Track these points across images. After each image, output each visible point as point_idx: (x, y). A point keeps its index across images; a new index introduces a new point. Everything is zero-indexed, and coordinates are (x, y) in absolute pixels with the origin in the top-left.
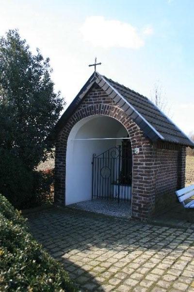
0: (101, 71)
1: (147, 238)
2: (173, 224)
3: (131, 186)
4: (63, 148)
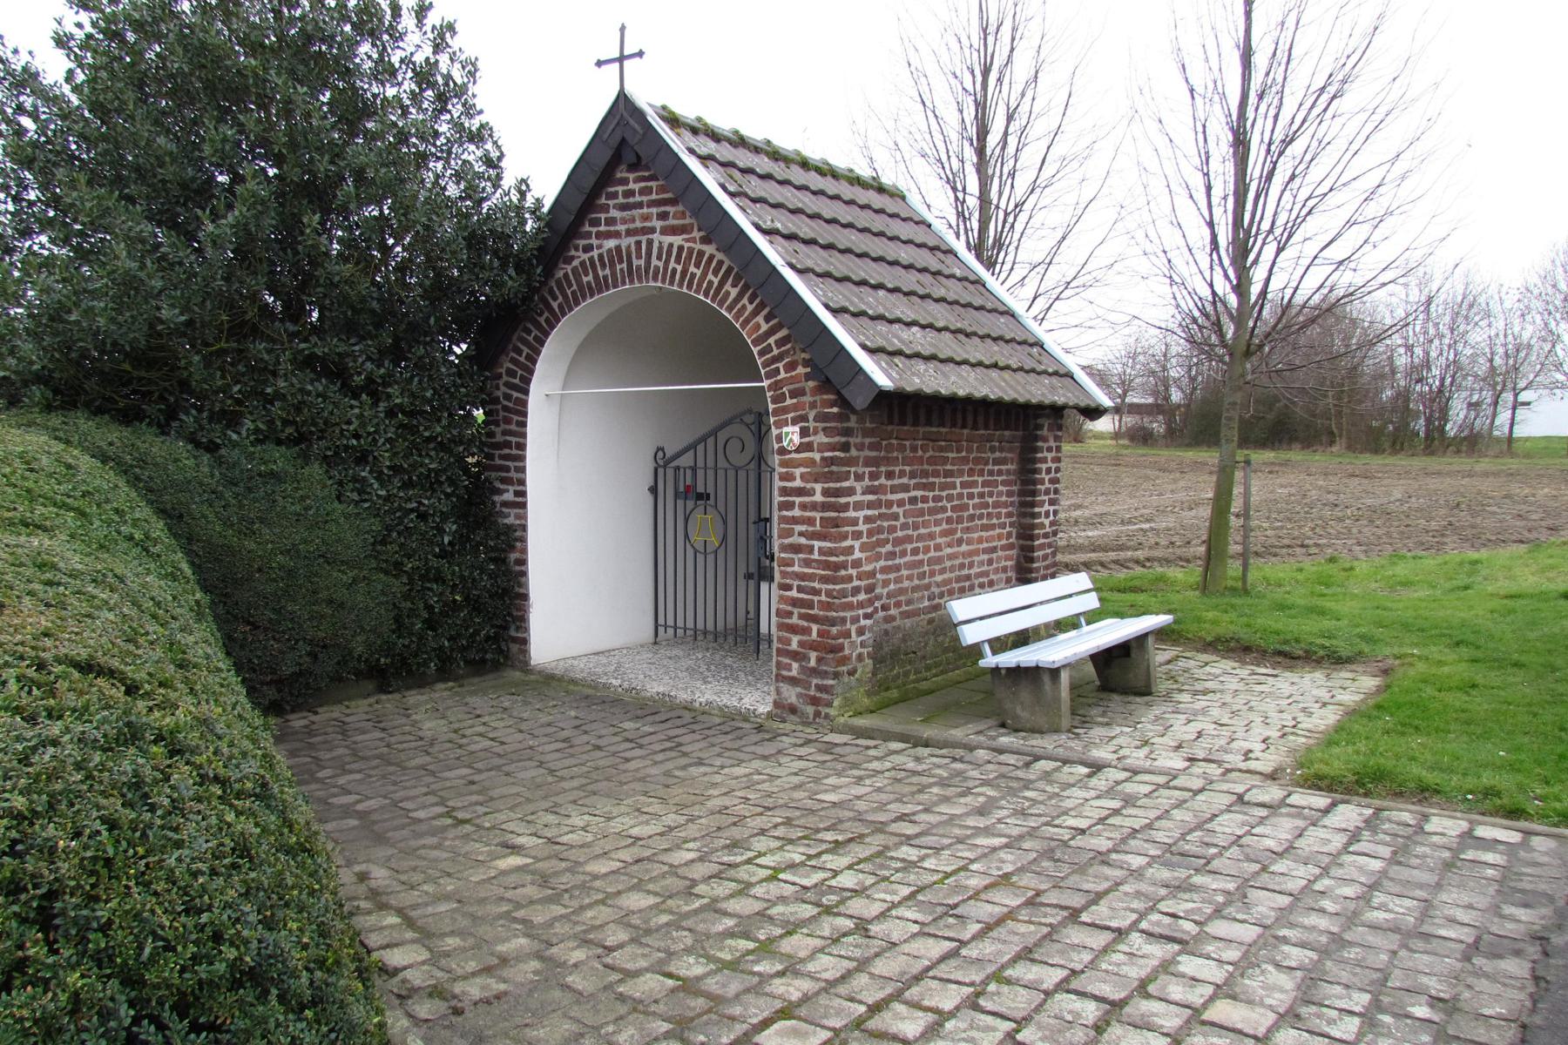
0: (646, 97)
2: (928, 732)
3: (771, 579)
4: (513, 427)
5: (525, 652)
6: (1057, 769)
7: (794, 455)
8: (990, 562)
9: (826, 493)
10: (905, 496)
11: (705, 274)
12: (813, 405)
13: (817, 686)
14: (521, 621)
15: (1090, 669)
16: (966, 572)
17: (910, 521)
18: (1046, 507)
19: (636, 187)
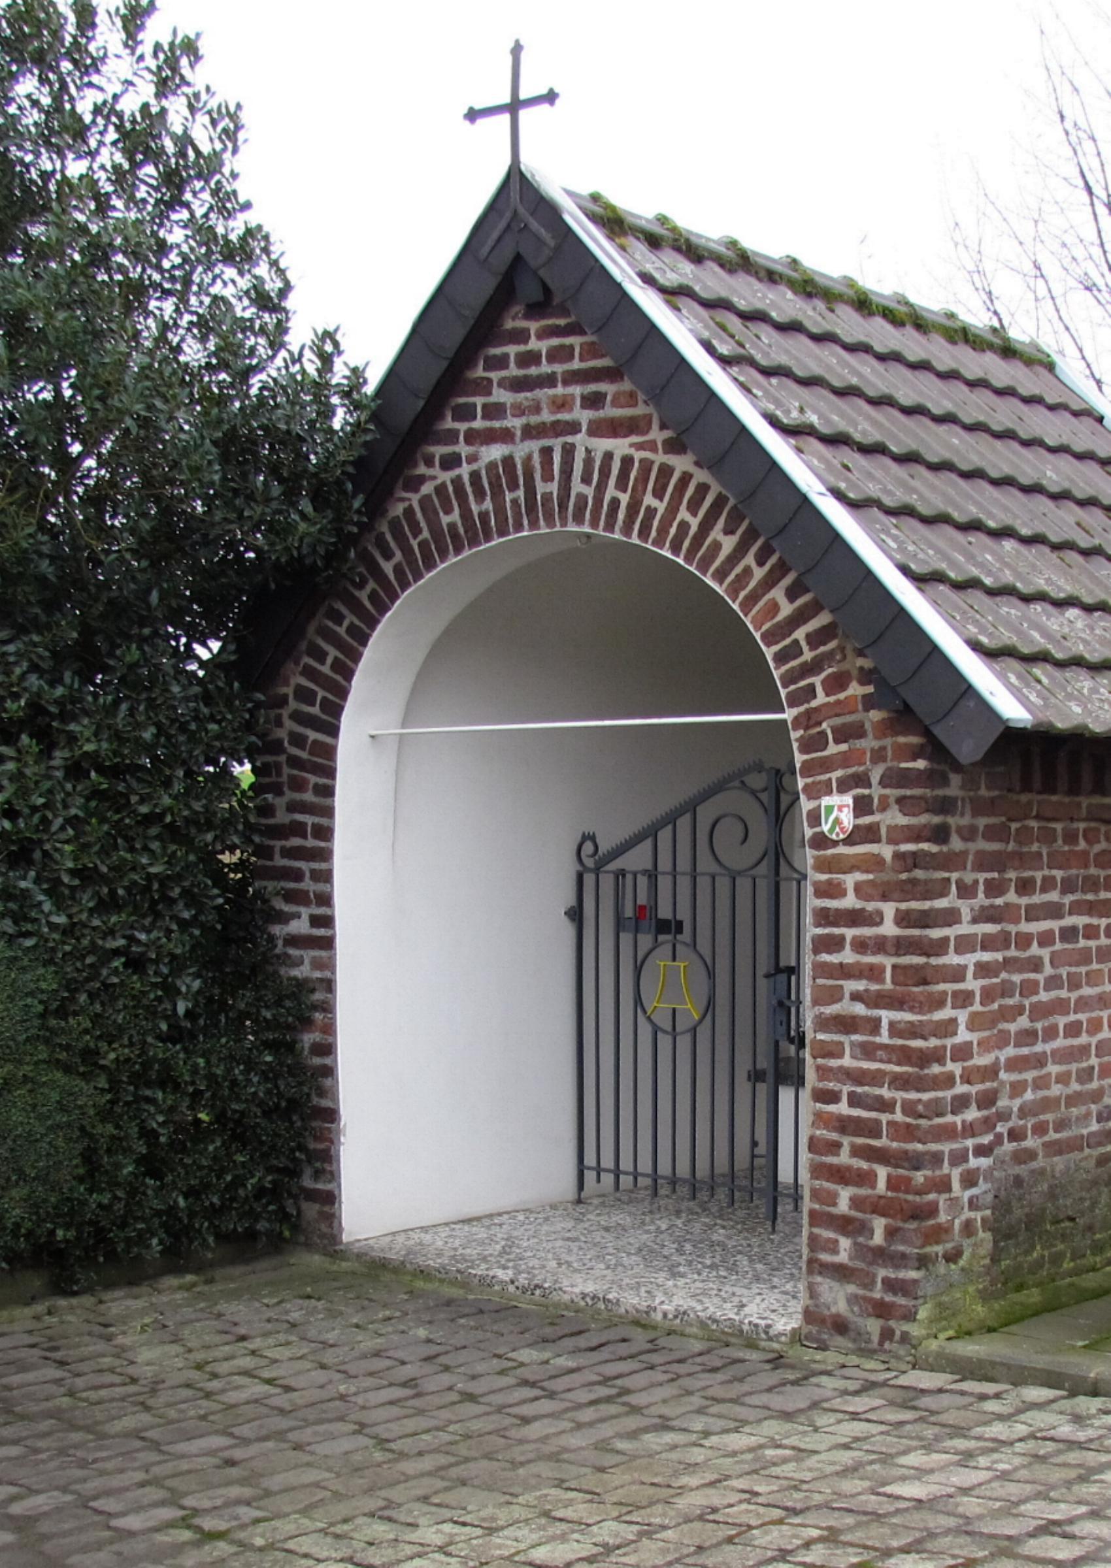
1: (232, 1401)
4: (309, 797)
7: (842, 850)
9: (903, 919)
10: (1054, 925)
11: (672, 510)
12: (878, 756)
13: (886, 1281)
17: (1064, 972)
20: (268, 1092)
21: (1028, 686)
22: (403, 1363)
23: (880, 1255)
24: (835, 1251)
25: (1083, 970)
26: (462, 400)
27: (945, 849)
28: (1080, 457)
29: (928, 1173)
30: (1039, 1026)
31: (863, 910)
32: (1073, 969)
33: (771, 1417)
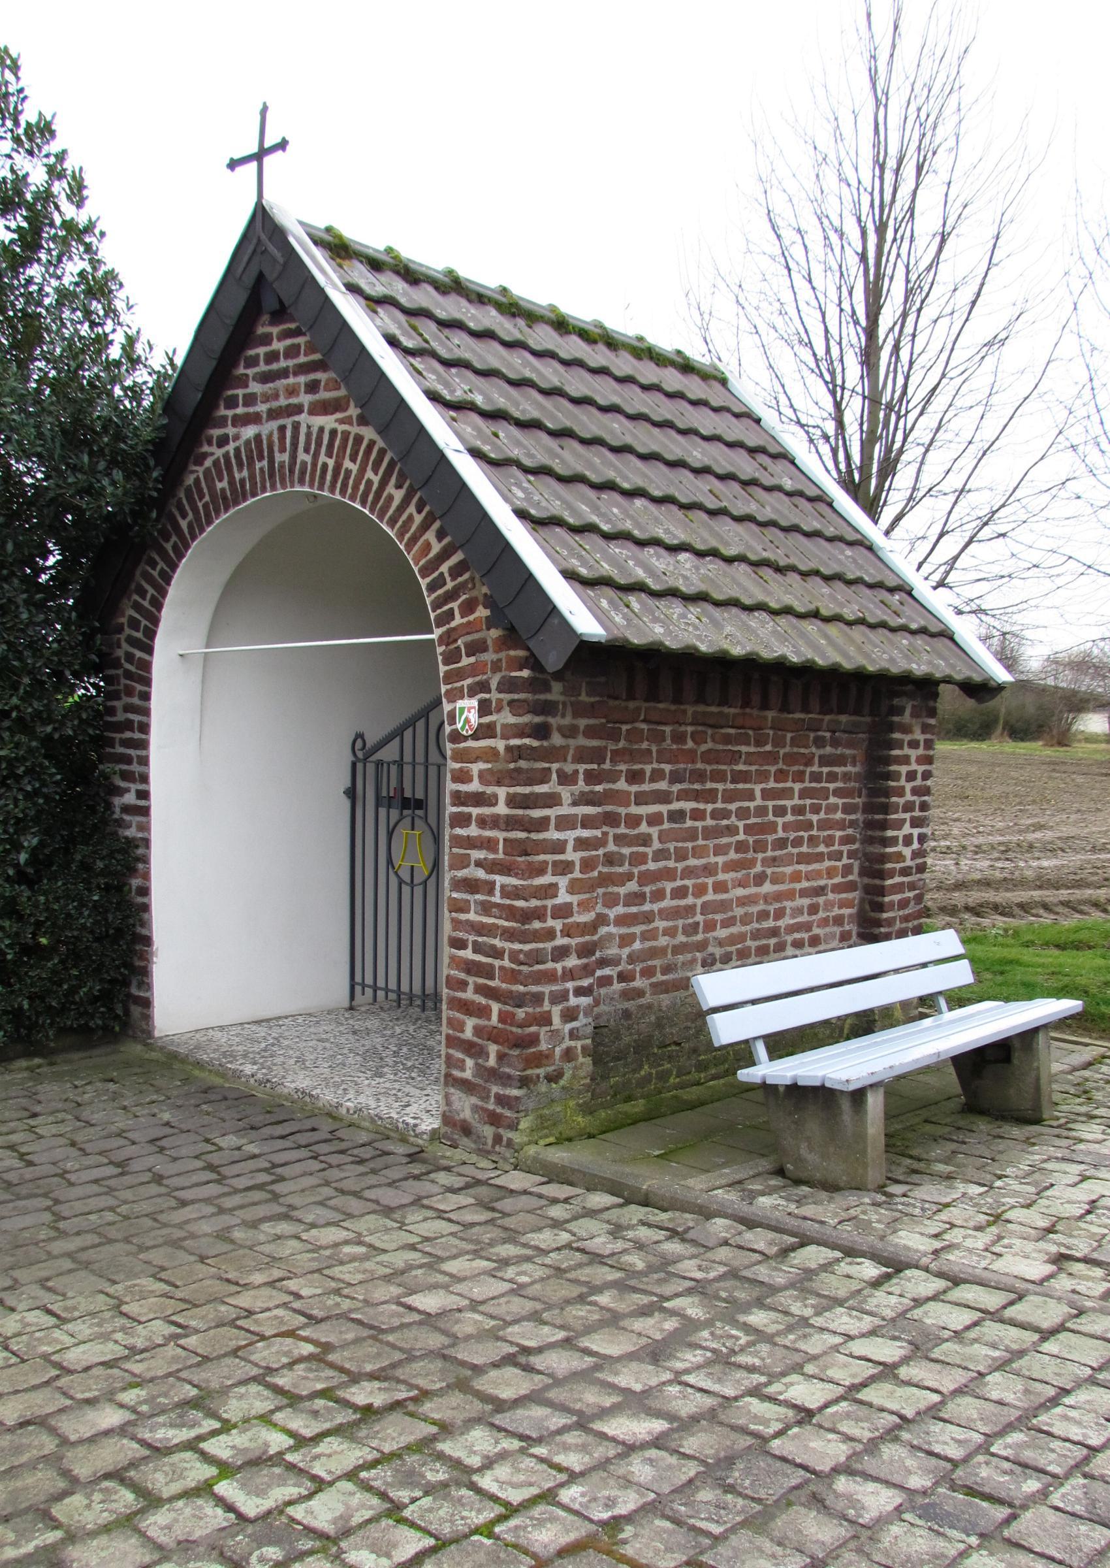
2: (651, 1180)
4: (136, 701)
5: (148, 1018)
6: (827, 1267)
7: (471, 744)
8: (813, 909)
9: (512, 801)
10: (663, 809)
11: (362, 471)
12: (496, 667)
13: (498, 1096)
14: (143, 974)
15: (951, 1080)
16: (770, 923)
17: (671, 846)
18: (907, 829)
19: (278, 346)
20: (96, 923)
21: (616, 609)
22: (134, 1143)
23: (493, 1075)
24: (463, 1070)
25: (690, 845)
26: (230, 392)
27: (545, 744)
28: (731, 445)
29: (530, 1010)
30: (647, 889)
31: (483, 793)
32: (680, 845)
33: (374, 1212)
